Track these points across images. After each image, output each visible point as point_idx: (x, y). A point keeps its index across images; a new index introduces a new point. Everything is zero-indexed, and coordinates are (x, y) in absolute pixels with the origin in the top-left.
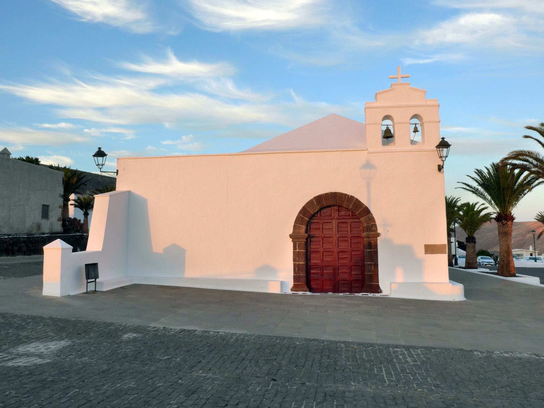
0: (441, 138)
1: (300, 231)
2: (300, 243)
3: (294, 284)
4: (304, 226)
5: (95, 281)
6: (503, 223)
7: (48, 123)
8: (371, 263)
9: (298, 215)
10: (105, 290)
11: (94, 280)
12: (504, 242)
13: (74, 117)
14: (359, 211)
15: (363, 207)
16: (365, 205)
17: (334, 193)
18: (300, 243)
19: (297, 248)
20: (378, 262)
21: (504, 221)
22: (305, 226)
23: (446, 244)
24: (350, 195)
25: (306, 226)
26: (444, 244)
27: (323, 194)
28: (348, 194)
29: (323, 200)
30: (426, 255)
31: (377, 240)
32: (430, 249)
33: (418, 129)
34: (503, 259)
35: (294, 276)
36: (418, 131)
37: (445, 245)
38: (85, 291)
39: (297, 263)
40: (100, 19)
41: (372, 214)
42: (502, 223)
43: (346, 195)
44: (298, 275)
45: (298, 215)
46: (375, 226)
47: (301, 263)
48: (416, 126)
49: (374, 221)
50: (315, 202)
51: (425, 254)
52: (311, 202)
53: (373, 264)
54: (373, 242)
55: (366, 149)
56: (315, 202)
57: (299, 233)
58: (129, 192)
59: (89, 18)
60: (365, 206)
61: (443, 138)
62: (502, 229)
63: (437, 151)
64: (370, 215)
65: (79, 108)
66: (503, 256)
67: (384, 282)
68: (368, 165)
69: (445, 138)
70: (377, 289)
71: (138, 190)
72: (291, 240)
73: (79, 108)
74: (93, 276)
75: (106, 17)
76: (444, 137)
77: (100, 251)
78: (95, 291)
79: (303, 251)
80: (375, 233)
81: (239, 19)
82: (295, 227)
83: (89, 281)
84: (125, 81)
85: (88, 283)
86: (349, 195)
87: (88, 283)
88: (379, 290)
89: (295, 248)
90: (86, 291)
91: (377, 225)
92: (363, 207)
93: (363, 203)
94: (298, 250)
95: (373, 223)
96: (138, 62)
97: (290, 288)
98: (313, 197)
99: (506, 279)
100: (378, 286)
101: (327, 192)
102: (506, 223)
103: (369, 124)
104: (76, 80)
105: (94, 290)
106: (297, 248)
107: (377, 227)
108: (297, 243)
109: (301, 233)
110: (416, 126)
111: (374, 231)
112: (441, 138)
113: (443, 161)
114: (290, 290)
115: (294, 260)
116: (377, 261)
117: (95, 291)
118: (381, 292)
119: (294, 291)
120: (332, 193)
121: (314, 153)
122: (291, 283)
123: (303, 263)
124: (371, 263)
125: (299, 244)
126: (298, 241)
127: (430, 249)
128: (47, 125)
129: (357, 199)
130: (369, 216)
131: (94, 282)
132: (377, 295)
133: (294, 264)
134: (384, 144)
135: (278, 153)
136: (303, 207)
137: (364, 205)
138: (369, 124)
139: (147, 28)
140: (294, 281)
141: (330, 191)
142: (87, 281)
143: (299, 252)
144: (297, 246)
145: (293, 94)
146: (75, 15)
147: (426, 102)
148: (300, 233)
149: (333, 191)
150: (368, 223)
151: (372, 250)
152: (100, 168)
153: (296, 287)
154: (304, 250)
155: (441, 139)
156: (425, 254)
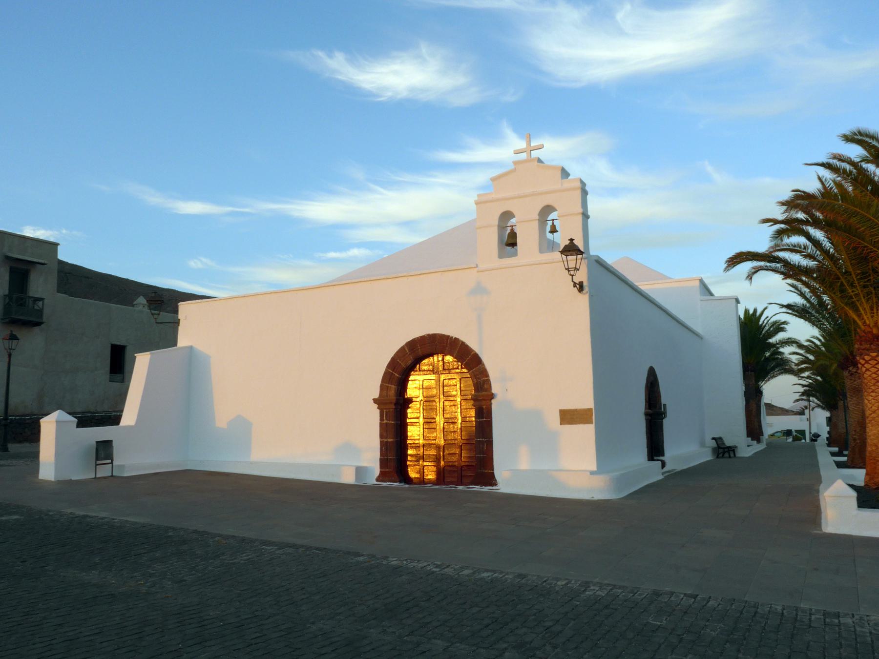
0: (569, 240)
1: (389, 393)
2: (388, 410)
3: (381, 471)
4: (393, 386)
5: (112, 463)
6: (850, 371)
7: (335, 251)
8: (483, 440)
9: (386, 369)
10: (126, 475)
11: (109, 461)
12: (855, 405)
13: (372, 240)
14: (467, 361)
15: (472, 354)
16: (475, 351)
17: (432, 334)
18: (388, 410)
19: (385, 418)
20: (492, 438)
21: (852, 367)
22: (395, 385)
23: (592, 409)
24: (454, 337)
25: (396, 386)
26: (588, 409)
27: (418, 338)
28: (451, 335)
29: (417, 347)
30: (562, 426)
31: (491, 404)
32: (569, 417)
33: (557, 229)
34: (854, 437)
35: (381, 460)
36: (557, 231)
37: (590, 410)
38: (94, 477)
39: (385, 440)
40: (404, 94)
41: (483, 365)
42: (849, 372)
43: (449, 336)
44: (386, 457)
45: (386, 370)
46: (488, 382)
47: (390, 440)
48: (553, 223)
49: (487, 375)
50: (407, 350)
51: (561, 424)
52: (402, 350)
53: (486, 441)
54: (486, 407)
55: (475, 266)
56: (407, 350)
57: (387, 396)
58: (191, 347)
59: (390, 94)
60: (474, 353)
61: (572, 240)
62: (849, 383)
63: (563, 263)
64: (481, 365)
65: (378, 225)
66: (855, 431)
67: (501, 471)
68: (479, 290)
69: (574, 240)
70: (490, 480)
71: (200, 346)
72: (376, 406)
73: (378, 225)
74: (102, 456)
75: (412, 89)
76: (573, 238)
77: (132, 426)
78: (112, 476)
79: (392, 422)
80: (489, 393)
81: (613, 62)
82: (382, 387)
83: (98, 462)
84: (442, 179)
85: (97, 465)
86: (452, 337)
87: (97, 465)
88: (493, 482)
89: (381, 419)
90: (111, 475)
91: (491, 381)
92: (472, 354)
93: (471, 348)
94: (385, 422)
95: (486, 378)
96: (458, 147)
97: (376, 478)
98: (405, 343)
99: (52, 459)
100: (492, 476)
101: (423, 334)
102: (855, 372)
103: (480, 228)
104: (372, 186)
105: (110, 475)
106: (385, 418)
107: (491, 384)
108: (384, 410)
109: (390, 396)
110: (553, 223)
111: (486, 390)
112: (569, 240)
113: (572, 276)
114: (375, 480)
115: (381, 436)
116: (491, 437)
117: (112, 476)
118: (495, 484)
119: (380, 481)
120: (429, 335)
121: (405, 279)
122: (376, 469)
123: (392, 440)
124: (483, 440)
125: (387, 413)
126: (385, 408)
127: (569, 417)
128: (332, 255)
129: (463, 343)
130: (480, 367)
131: (111, 465)
132: (486, 489)
133: (380, 441)
134: (501, 256)
135: (361, 282)
136: (392, 358)
137: (473, 351)
138: (480, 228)
139: (472, 96)
140: (381, 467)
141: (428, 333)
142: (96, 462)
143: (386, 423)
144: (385, 416)
145: (709, 169)
146: (369, 94)
147: (562, 185)
148: (388, 396)
149: (431, 332)
150: (479, 378)
151: (485, 419)
152: (156, 319)
153: (382, 477)
154: (393, 421)
155: (569, 241)
156: (561, 424)
